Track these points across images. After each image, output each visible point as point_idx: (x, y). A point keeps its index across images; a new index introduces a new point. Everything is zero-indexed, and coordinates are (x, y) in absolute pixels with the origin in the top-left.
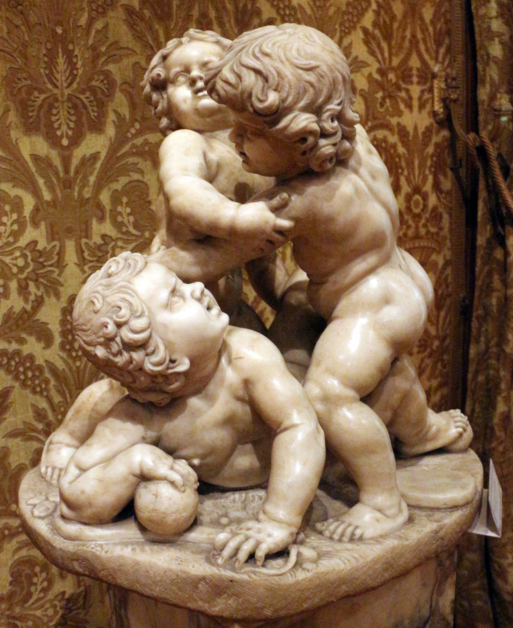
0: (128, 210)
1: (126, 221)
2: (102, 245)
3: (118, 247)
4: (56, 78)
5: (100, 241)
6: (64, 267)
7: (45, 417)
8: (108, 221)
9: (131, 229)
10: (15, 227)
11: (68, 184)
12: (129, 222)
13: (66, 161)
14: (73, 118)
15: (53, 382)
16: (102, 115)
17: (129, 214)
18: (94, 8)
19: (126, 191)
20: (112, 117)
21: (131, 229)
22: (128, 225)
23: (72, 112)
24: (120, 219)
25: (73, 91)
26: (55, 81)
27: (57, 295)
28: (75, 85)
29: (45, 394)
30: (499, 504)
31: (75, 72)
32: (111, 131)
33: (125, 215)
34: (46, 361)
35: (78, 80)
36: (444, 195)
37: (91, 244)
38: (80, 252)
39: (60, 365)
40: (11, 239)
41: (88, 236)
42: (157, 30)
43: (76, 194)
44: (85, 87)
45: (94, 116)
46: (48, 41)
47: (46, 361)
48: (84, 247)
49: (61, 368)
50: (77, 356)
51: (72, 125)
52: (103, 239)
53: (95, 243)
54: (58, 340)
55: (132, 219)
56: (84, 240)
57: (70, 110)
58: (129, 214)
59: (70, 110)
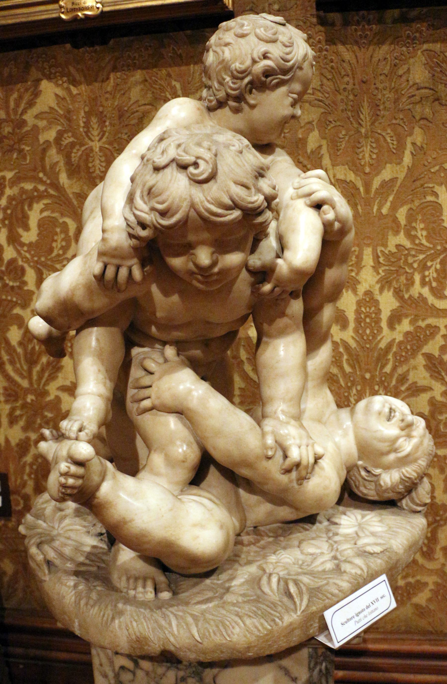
0: (422, 226)
1: (419, 234)
2: (395, 253)
3: (411, 255)
4: (92, 134)
5: (394, 250)
6: (361, 268)
7: (338, 382)
8: (402, 233)
9: (424, 242)
10: (64, 244)
11: (368, 203)
12: (422, 235)
13: (367, 186)
14: (376, 151)
15: (345, 357)
16: (401, 146)
17: (422, 229)
18: (119, 77)
19: (422, 208)
20: (409, 146)
21: (424, 242)
22: (421, 238)
23: (374, 145)
24: (413, 233)
25: (104, 143)
26: (360, 121)
27: (355, 291)
28: (104, 139)
29: (397, 364)
30: (369, 618)
31: (105, 129)
32: (407, 159)
33: (419, 231)
34: (341, 339)
35: (107, 134)
36: (25, 248)
37: (387, 252)
38: (376, 257)
39: (353, 344)
40: (61, 252)
41: (385, 246)
42: (175, 85)
43: (375, 210)
44: (112, 139)
45: (393, 148)
46: (86, 105)
47: (341, 339)
48: (380, 254)
49: (353, 347)
50: (368, 339)
51: (374, 156)
52: (397, 248)
53: (390, 251)
54: (352, 325)
55: (424, 233)
56: (379, 249)
57: (372, 144)
58: (422, 229)
59: (372, 144)
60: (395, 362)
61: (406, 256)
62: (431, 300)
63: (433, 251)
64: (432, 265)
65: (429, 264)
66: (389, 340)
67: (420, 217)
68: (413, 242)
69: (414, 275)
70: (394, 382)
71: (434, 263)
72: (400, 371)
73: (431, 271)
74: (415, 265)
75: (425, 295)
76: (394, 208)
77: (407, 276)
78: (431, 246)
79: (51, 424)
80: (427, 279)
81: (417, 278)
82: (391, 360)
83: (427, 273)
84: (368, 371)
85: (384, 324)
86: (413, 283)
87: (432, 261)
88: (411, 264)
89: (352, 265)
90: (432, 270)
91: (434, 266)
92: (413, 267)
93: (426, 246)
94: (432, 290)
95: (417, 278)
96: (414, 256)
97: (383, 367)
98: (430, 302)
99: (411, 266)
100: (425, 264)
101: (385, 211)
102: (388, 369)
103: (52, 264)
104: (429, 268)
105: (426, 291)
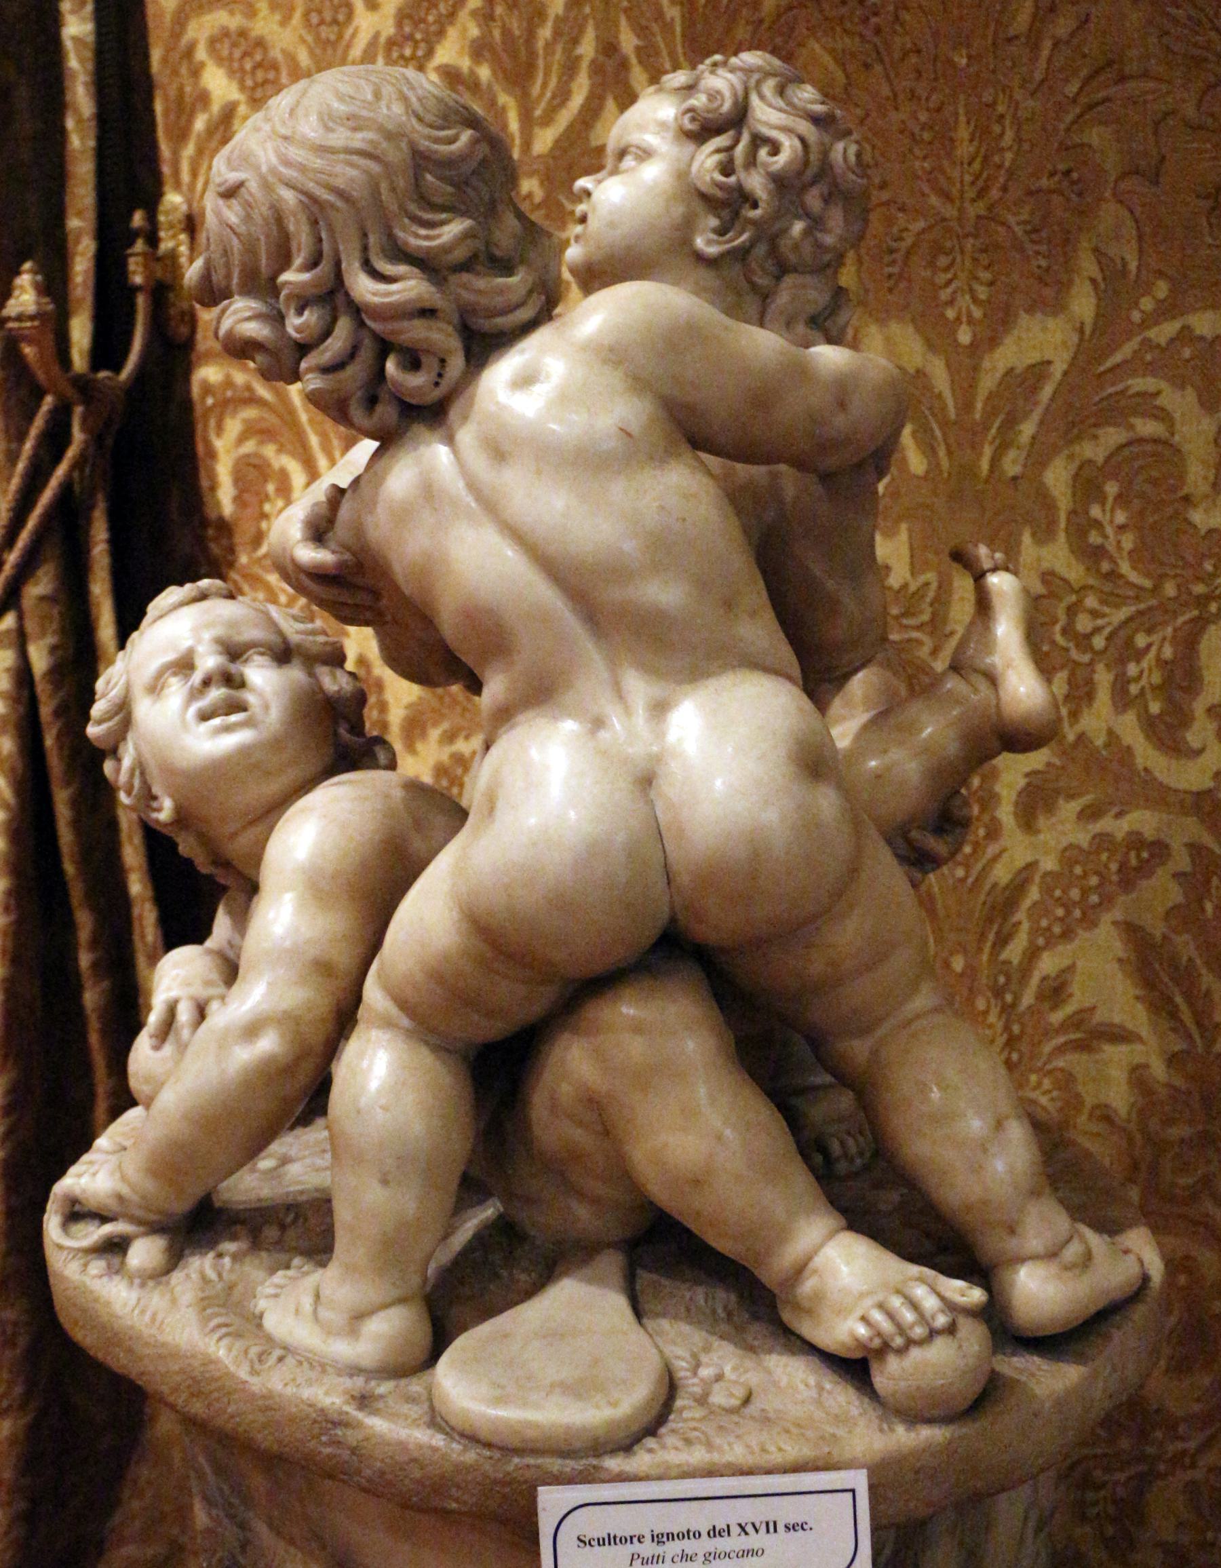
0: (1121, 517)
17: (1122, 528)
24: (1094, 538)
60: (1035, 931)
61: (1072, 611)
62: (1146, 755)
63: (1153, 602)
64: (1149, 646)
65: (1141, 640)
66: (1020, 863)
67: (1112, 489)
68: (1093, 568)
69: (1093, 671)
70: (1028, 999)
71: (1155, 638)
72: (1048, 964)
73: (1145, 664)
74: (1099, 642)
75: (1127, 740)
76: (1039, 458)
77: (1072, 674)
78: (1147, 583)
79: (758, 142)
80: (1134, 689)
81: (1103, 678)
82: (1025, 926)
83: (1132, 669)
84: (962, 948)
85: (1005, 813)
86: (1090, 696)
87: (1149, 631)
88: (1088, 636)
89: (919, 628)
90: (1149, 660)
91: (1154, 650)
92: (1089, 648)
93: (1134, 585)
94: (1150, 725)
95: (1103, 678)
96: (1095, 614)
97: (1003, 940)
98: (1140, 762)
99: (1084, 641)
100: (1129, 642)
101: (1012, 465)
102: (1014, 952)
103: (550, 24)
104: (1139, 655)
105: (1129, 729)
